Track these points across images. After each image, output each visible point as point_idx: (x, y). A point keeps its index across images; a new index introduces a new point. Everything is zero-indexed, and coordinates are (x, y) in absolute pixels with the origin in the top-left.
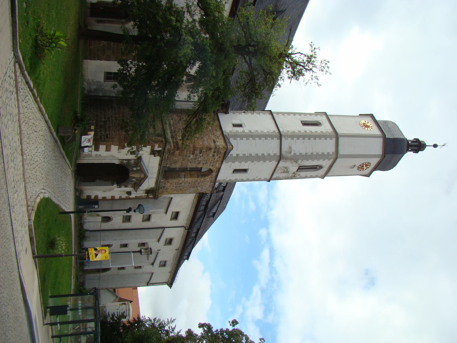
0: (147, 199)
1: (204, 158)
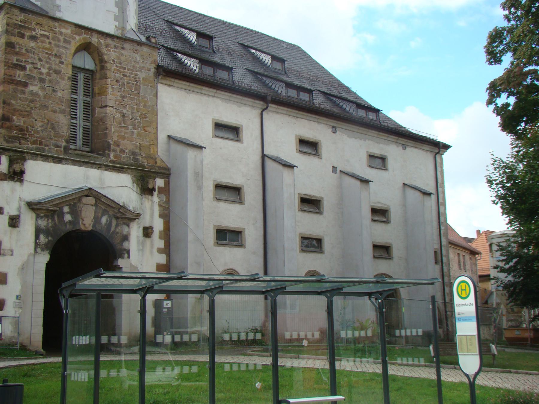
0: (169, 192)
1: (40, 60)
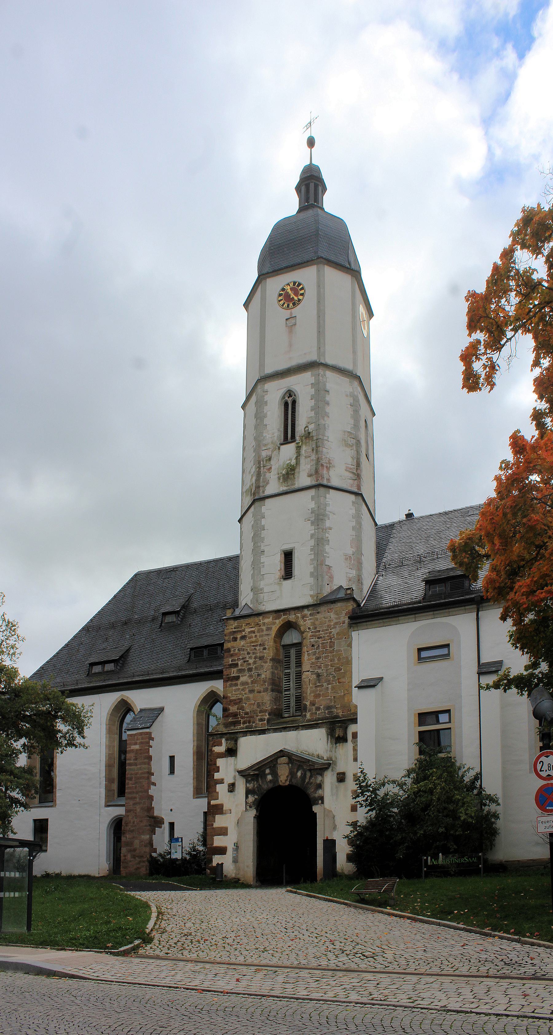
1: (248, 653)
